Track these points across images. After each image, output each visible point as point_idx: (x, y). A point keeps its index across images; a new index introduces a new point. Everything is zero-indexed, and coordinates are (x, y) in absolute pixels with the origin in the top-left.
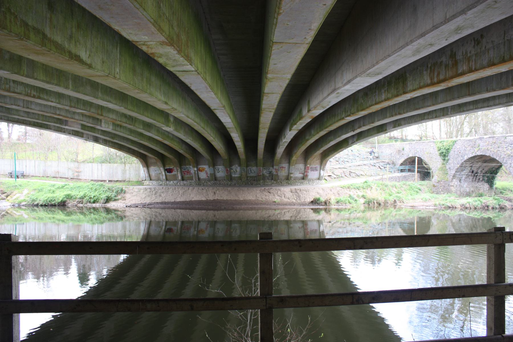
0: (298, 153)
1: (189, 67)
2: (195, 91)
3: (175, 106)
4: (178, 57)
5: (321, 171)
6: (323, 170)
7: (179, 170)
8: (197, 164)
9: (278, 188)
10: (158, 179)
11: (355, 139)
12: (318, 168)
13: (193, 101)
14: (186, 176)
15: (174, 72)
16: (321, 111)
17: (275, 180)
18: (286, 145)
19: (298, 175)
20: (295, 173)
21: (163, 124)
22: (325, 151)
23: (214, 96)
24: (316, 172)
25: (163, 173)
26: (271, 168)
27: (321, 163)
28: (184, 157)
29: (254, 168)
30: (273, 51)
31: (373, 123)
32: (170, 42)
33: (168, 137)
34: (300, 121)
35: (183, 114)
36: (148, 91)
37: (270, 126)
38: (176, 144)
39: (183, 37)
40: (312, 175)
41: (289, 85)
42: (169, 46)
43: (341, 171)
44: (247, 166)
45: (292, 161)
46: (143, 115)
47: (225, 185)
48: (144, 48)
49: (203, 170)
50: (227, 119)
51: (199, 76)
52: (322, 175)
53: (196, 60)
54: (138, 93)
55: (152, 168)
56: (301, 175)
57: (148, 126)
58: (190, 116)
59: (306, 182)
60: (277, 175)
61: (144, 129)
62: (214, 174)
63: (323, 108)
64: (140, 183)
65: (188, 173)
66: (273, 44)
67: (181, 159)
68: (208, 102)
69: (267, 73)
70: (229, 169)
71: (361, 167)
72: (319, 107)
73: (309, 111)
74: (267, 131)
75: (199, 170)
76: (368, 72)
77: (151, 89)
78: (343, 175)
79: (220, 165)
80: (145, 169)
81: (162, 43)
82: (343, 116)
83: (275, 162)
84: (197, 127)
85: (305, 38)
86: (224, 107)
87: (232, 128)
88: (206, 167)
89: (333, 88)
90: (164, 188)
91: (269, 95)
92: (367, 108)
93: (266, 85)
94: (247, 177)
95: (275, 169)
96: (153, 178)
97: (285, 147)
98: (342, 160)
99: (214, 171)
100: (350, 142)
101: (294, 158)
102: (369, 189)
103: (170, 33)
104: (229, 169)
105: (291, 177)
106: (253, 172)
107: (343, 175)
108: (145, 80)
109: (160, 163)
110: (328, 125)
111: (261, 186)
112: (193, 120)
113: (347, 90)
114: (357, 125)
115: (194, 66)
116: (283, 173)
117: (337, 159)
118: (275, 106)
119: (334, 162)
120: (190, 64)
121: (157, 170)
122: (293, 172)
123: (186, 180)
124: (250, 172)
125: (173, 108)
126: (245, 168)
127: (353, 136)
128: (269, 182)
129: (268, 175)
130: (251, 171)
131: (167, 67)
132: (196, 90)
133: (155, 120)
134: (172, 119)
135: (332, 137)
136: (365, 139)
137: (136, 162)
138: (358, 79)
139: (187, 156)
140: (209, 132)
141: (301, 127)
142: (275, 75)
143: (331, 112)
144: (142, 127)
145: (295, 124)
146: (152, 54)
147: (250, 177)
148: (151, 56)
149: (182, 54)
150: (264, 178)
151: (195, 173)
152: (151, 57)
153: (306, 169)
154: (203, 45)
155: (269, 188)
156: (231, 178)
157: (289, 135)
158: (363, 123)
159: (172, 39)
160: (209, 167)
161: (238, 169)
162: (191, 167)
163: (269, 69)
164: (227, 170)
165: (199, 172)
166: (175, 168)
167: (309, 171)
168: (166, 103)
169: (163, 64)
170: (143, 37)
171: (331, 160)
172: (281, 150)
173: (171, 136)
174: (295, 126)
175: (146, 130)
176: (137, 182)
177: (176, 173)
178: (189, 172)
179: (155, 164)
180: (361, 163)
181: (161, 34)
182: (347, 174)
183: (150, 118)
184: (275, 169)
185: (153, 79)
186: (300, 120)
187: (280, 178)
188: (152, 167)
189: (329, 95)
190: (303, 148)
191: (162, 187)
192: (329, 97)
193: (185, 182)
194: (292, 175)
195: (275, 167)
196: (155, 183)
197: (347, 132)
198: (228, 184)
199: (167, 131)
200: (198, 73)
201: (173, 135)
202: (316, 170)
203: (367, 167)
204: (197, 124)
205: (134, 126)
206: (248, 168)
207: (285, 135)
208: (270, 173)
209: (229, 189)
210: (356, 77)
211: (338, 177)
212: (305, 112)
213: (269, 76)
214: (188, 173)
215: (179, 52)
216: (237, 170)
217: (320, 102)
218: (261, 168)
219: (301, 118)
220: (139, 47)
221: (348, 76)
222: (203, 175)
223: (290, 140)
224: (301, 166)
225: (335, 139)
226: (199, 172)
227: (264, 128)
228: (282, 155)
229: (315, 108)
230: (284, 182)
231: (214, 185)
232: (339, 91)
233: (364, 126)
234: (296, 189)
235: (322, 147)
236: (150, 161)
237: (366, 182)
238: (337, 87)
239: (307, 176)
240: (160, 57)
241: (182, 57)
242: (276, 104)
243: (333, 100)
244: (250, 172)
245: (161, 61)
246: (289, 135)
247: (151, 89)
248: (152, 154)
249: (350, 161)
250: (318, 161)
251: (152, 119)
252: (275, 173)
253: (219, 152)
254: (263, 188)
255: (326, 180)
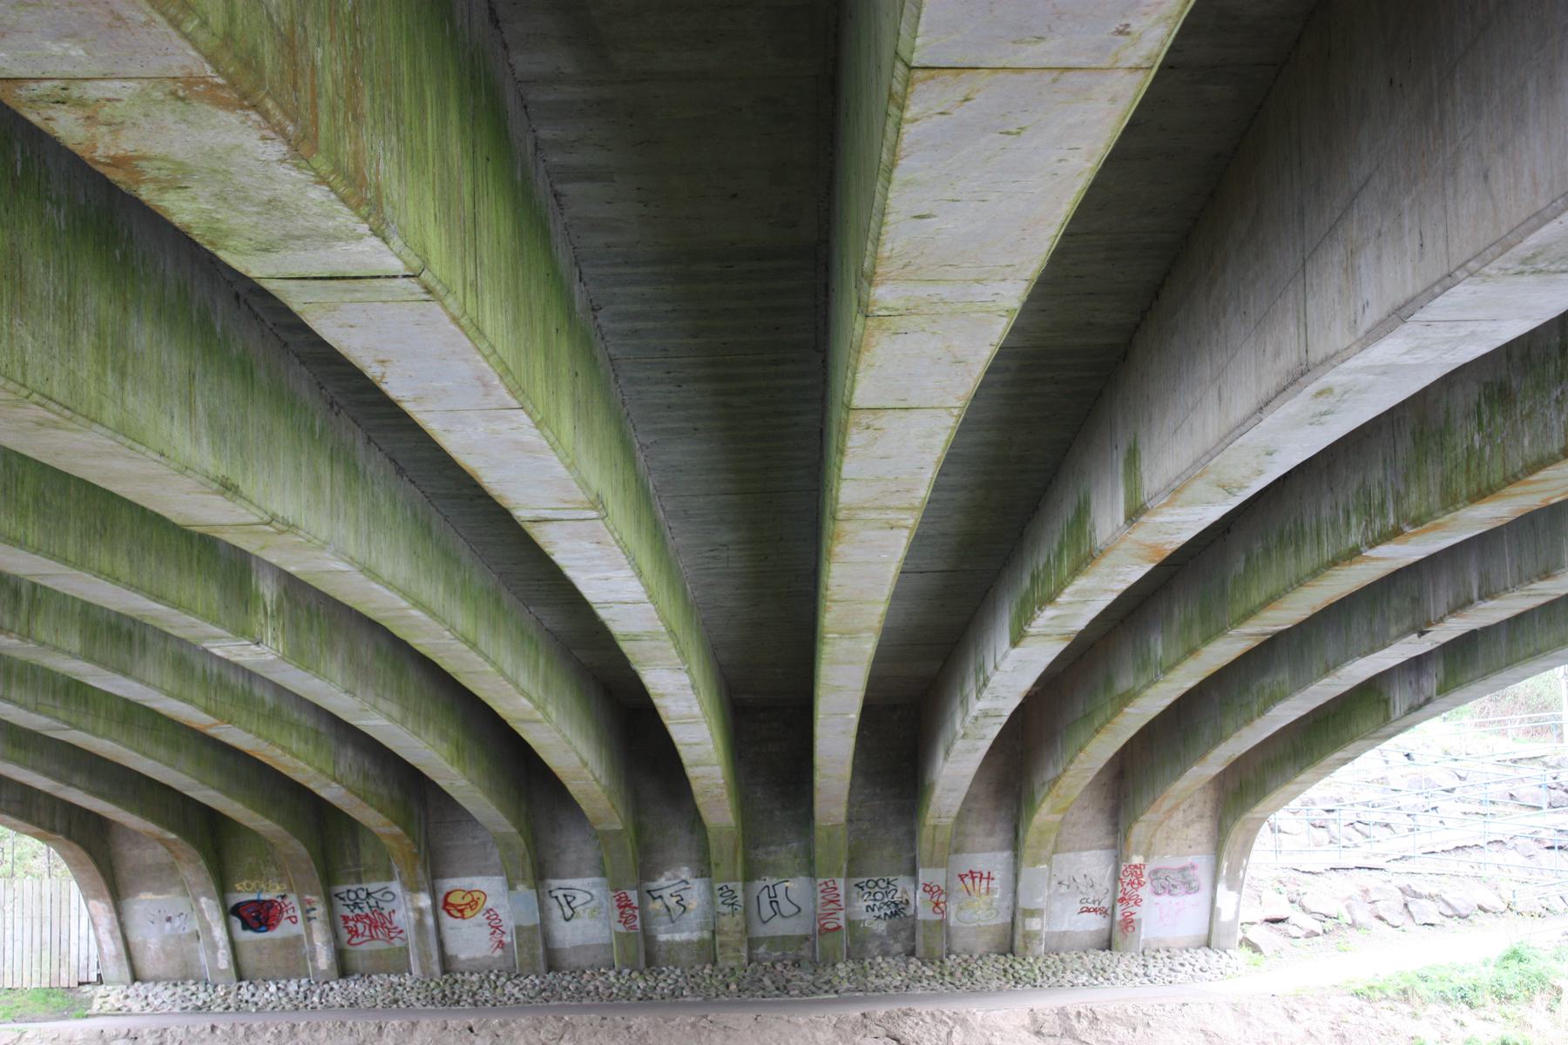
0: (1065, 782)
1: (368, 253)
2: (408, 407)
3: (286, 505)
4: (291, 182)
5: (1221, 888)
6: (1235, 884)
7: (320, 910)
8: (432, 865)
9: (949, 1008)
10: (186, 974)
11: (1430, 684)
12: (1202, 876)
13: (400, 471)
14: (364, 947)
15: (271, 286)
16: (1214, 513)
17: (929, 959)
18: (994, 731)
19: (1066, 919)
20: (1057, 906)
21: (216, 622)
22: (1237, 767)
23: (532, 436)
24: (1190, 899)
25: (219, 933)
26: (902, 882)
27: (1218, 846)
28: (352, 825)
29: (796, 887)
30: (906, 128)
31: (1546, 575)
32: (233, 84)
33: (247, 701)
34: (1081, 582)
35: (340, 554)
36: (110, 413)
37: (889, 614)
38: (295, 744)
39: (327, 58)
40: (1165, 916)
41: (1004, 353)
42: (226, 105)
43: (1347, 885)
44: (750, 876)
45: (1030, 836)
46: (81, 564)
47: (609, 1001)
48: (66, 126)
49: (473, 904)
50: (619, 583)
51: (436, 307)
52: (1226, 915)
53: (415, 203)
54: (40, 424)
55: (145, 905)
56: (1094, 924)
57: (118, 636)
58: (386, 570)
59: (1123, 963)
60: (943, 923)
61: (89, 658)
62: (544, 931)
63: (1228, 490)
64: (67, 999)
65: (374, 925)
66: (908, 82)
67: (327, 837)
68: (493, 479)
69: (870, 279)
70: (633, 896)
71: (1475, 855)
72: (1198, 488)
73: (1135, 513)
74: (868, 646)
75: (444, 905)
76: (1532, 241)
77: (131, 401)
78: (1363, 915)
79: (577, 874)
80: (102, 909)
81: (185, 90)
82: (1355, 538)
83: (924, 846)
84: (429, 638)
85: (1123, 31)
86: (597, 503)
87: (653, 636)
88: (490, 886)
89: (1290, 358)
90: (223, 1026)
91: (882, 421)
92: (1512, 479)
93: (866, 357)
94: (753, 943)
95: (928, 889)
96: (148, 965)
97: (985, 745)
98: (1348, 815)
99: (542, 908)
100: (1400, 698)
101: (1044, 815)
102: (1540, 1001)
103: (232, 19)
104: (633, 896)
105: (1029, 936)
106: (787, 908)
107: (1363, 915)
108: (86, 339)
109: (194, 871)
110: (1256, 597)
111: (844, 1001)
112: (405, 595)
113: (1386, 370)
114: (1442, 596)
115: (397, 242)
116: (977, 914)
117: (1317, 814)
118: (923, 492)
119: (1298, 828)
120: (375, 232)
121: (180, 914)
122: (1040, 902)
123: (366, 975)
124: (767, 911)
125: (274, 518)
126: (738, 886)
127: (1416, 665)
128: (891, 971)
129: (881, 927)
130: (773, 901)
131: (221, 254)
132: (417, 399)
133: (159, 598)
134: (268, 590)
135: (1284, 675)
136: (1494, 680)
137: (40, 864)
138: (1462, 292)
139: (369, 816)
140: (507, 660)
141: (1081, 617)
142: (922, 291)
143: (1268, 519)
144: (75, 643)
145: (1050, 600)
146: (118, 162)
147: (773, 941)
148: (116, 176)
149: (320, 162)
150: (858, 945)
151: (420, 924)
152: (110, 187)
153: (1124, 881)
154: (453, 116)
155: (894, 1008)
156: (649, 955)
157: (1009, 670)
158: (1484, 578)
159: (250, 61)
160: (511, 887)
161: (696, 894)
162: (395, 887)
163: (885, 251)
164: (623, 904)
165: (447, 921)
166: (292, 899)
167: (1144, 892)
168: (228, 488)
169: (197, 233)
170: (56, 49)
171: (1281, 817)
172: (957, 765)
173: (269, 697)
174: (1049, 612)
175: (103, 664)
176: (50, 991)
177: (299, 928)
178: (379, 922)
179: (163, 877)
180: (1472, 832)
181: (175, 24)
182: (1390, 905)
183: (130, 586)
184: (928, 889)
185: (143, 335)
186: (1076, 571)
187: (958, 945)
188: (146, 896)
189: (1263, 406)
190: (1100, 748)
191: (205, 1022)
192: (1269, 420)
193: (356, 987)
194: (1034, 924)
195: (924, 875)
196: (161, 994)
197: (1379, 642)
198: (629, 993)
199: (237, 667)
200: (428, 291)
201: (279, 690)
202: (1190, 888)
203: (1512, 858)
204: (433, 614)
205: (27, 636)
206: (759, 884)
207: (981, 668)
208: (898, 911)
209: (640, 1021)
210: (1447, 281)
211: (1329, 926)
212: (1107, 519)
213: (883, 295)
214: (374, 925)
215: (301, 148)
216: (685, 901)
217: (1210, 454)
218: (841, 883)
219: (1085, 560)
220: (33, 118)
221: (1386, 276)
222: (470, 940)
223: (1014, 702)
224: (1092, 864)
225: (1300, 684)
226: (447, 921)
227: (853, 634)
228: (970, 797)
229: (1175, 491)
230: (989, 969)
231: (546, 998)
232: (1331, 378)
233: (1487, 594)
234: (1062, 1013)
235: (1219, 739)
236: (133, 856)
237: (1516, 955)
238: (1318, 352)
239: (1129, 923)
240: (174, 185)
241: (322, 180)
242: (929, 474)
243: (1291, 438)
244: (767, 911)
245: (183, 209)
246: (1009, 670)
247: (131, 401)
248: (143, 813)
249: (1397, 819)
250: (1199, 832)
251: (138, 589)
252: (925, 913)
253: (572, 788)
254: (855, 1013)
255: (1255, 948)
